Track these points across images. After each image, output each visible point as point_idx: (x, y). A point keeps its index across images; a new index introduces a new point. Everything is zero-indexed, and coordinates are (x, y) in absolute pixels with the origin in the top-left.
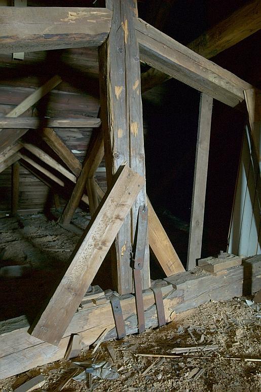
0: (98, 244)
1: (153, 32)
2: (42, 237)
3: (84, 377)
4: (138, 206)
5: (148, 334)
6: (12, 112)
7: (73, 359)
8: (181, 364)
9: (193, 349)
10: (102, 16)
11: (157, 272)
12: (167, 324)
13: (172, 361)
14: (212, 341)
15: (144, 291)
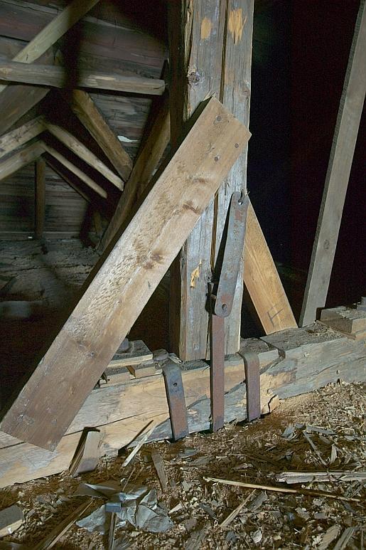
0: (145, 257)
2: (69, 267)
3: (100, 521)
4: (230, 191)
5: (230, 435)
6: (21, 55)
7: (86, 475)
8: (302, 511)
9: (322, 477)
11: (252, 326)
12: (263, 416)
13: (281, 500)
14: (353, 461)
15: (227, 358)
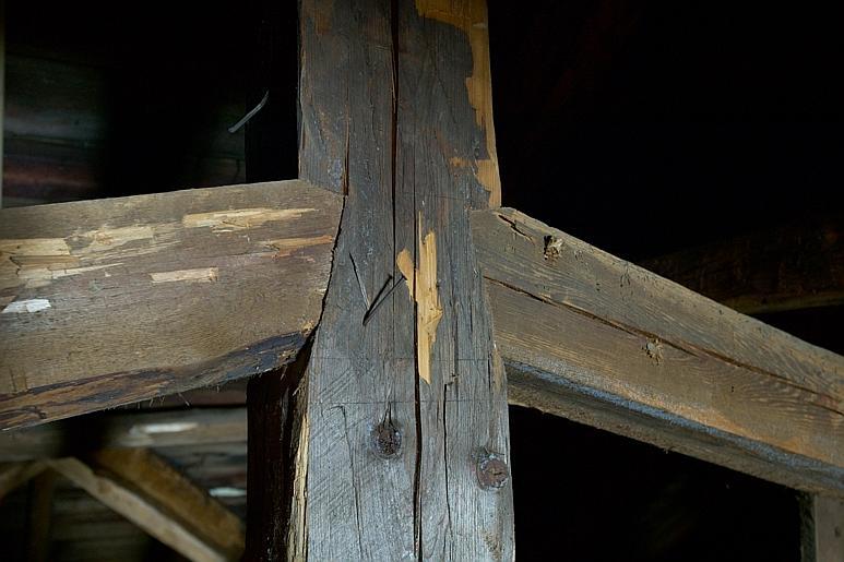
1: (585, 274)
10: (270, 229)
